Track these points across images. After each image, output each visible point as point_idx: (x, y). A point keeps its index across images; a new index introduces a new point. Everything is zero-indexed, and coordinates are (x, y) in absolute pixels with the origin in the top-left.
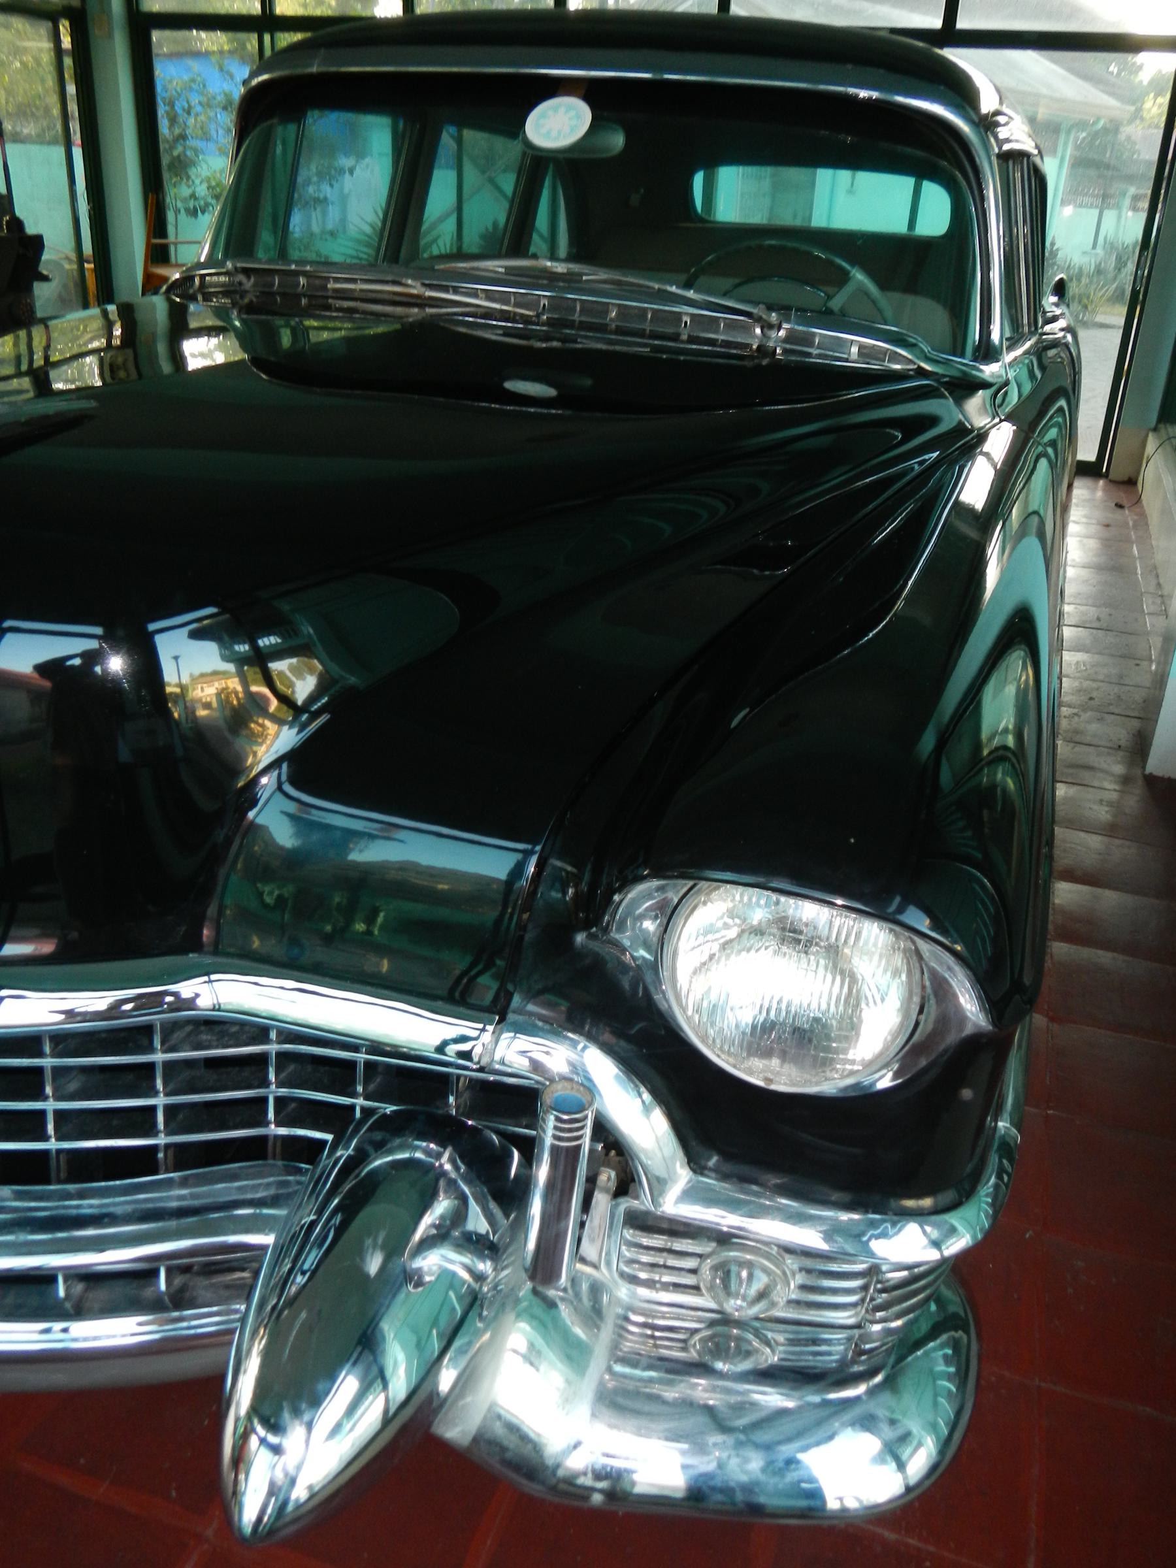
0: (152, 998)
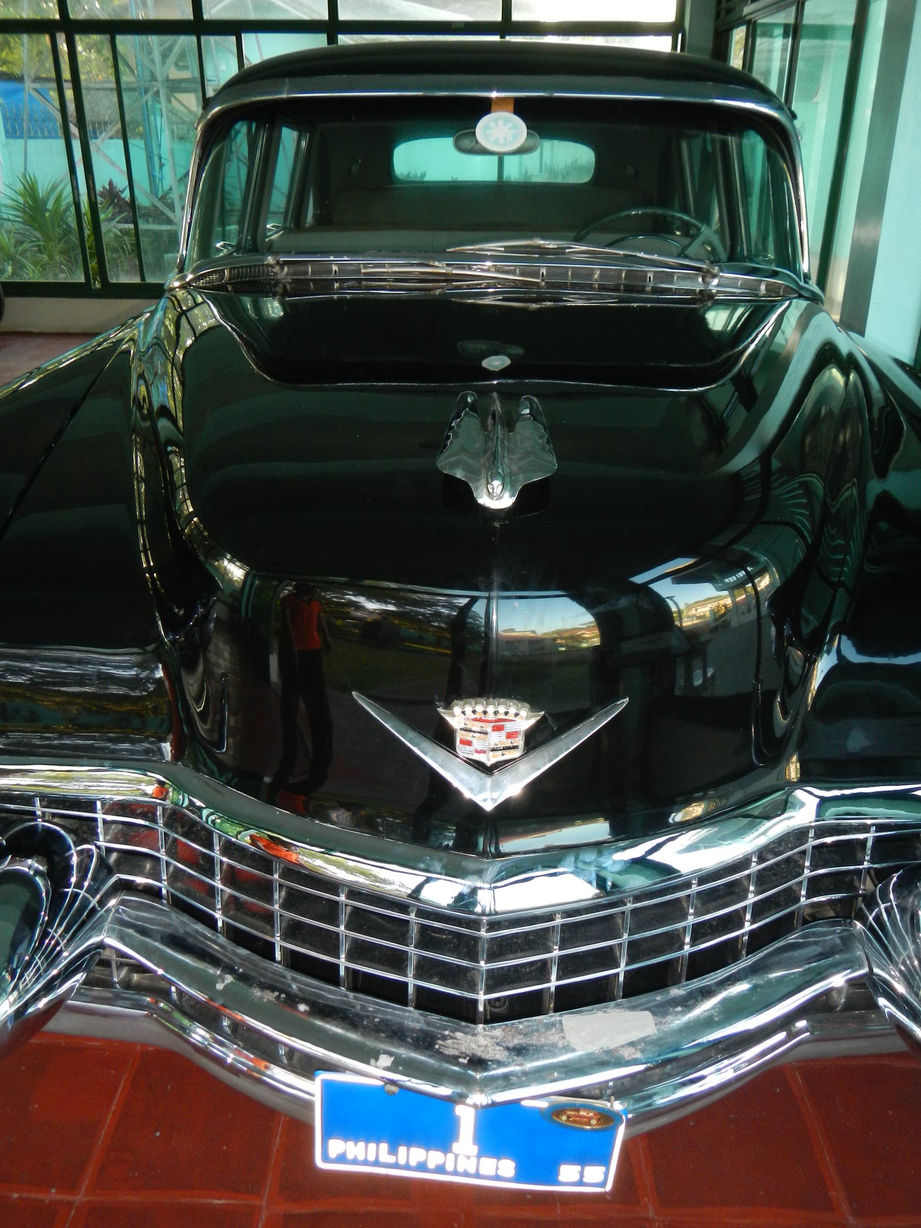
0: (411, 864)
